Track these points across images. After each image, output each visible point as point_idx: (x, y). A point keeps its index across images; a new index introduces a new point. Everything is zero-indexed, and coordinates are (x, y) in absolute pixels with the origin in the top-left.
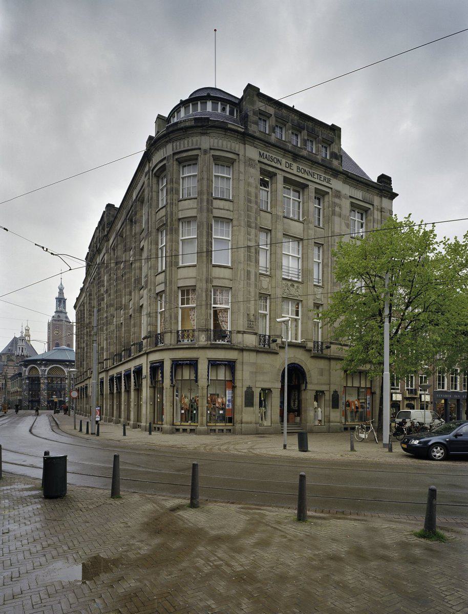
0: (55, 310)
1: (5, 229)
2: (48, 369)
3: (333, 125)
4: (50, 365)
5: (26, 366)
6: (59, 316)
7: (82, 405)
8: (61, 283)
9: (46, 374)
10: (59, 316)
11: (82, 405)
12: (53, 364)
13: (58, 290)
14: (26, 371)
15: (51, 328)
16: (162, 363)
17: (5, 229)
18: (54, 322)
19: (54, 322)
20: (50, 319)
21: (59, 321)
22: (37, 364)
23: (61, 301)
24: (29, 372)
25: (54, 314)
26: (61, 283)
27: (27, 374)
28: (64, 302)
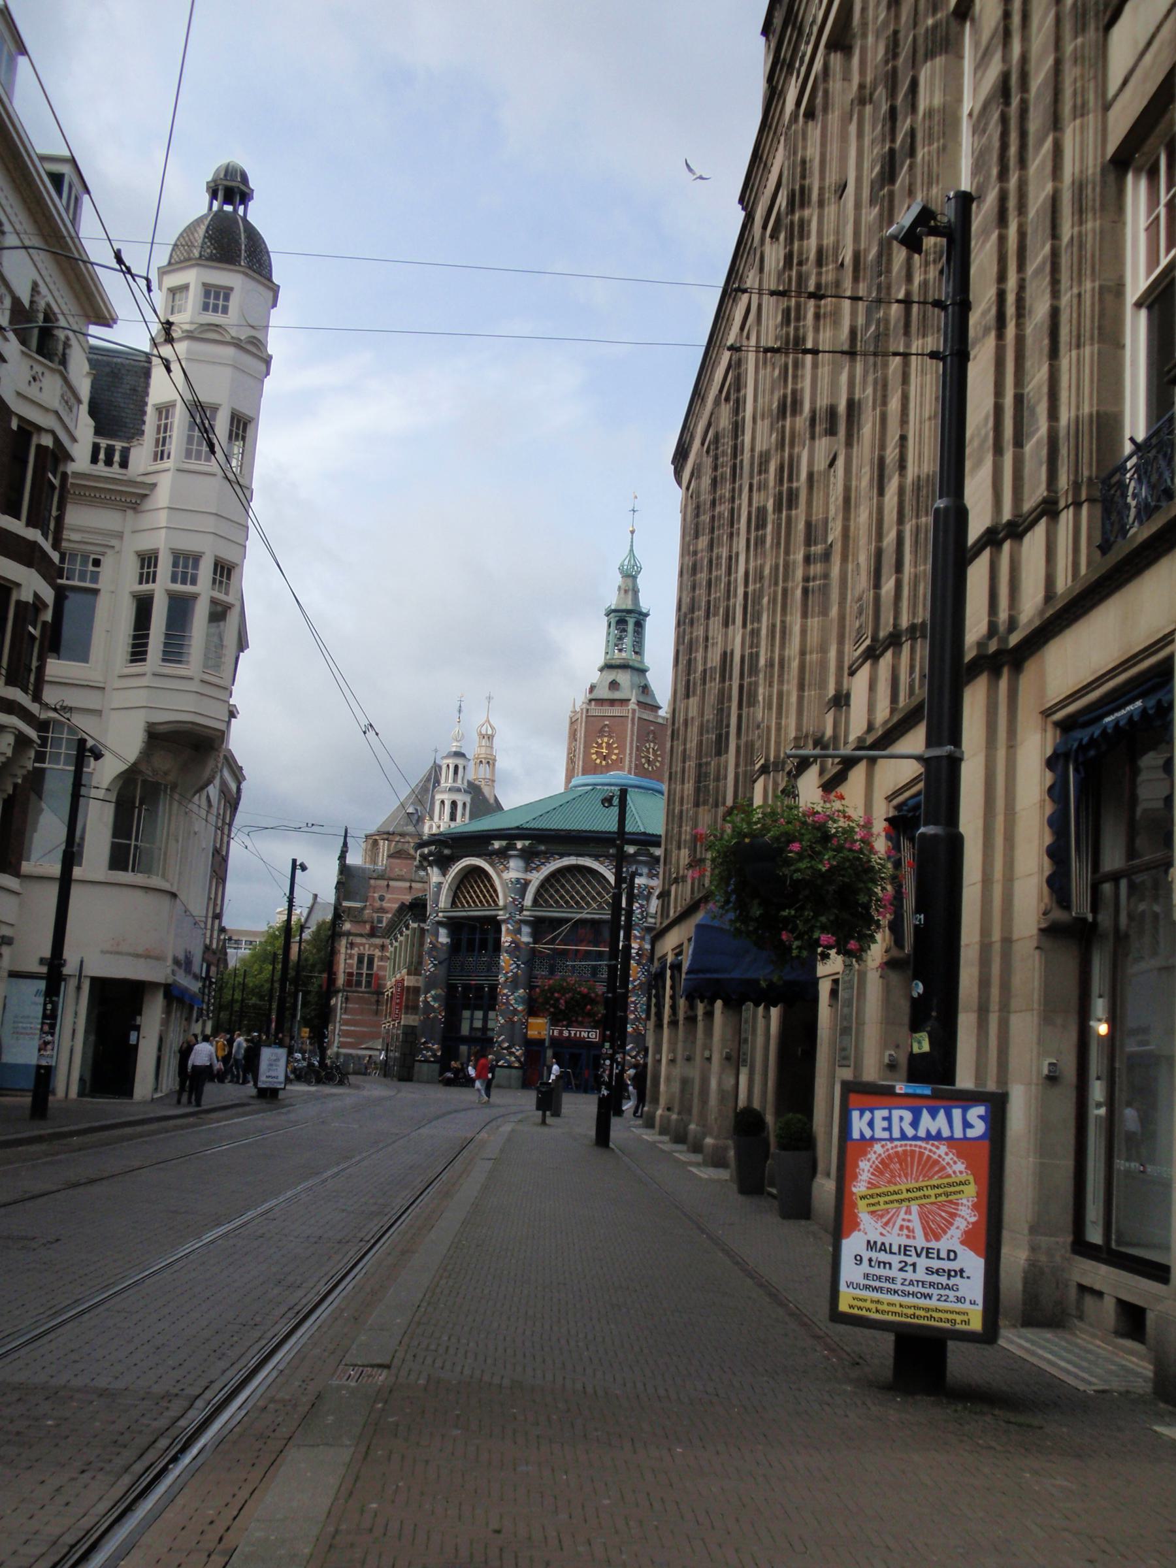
0: (601, 662)
1: (460, 711)
2: (536, 878)
3: (673, 463)
4: (548, 856)
5: (443, 864)
6: (614, 685)
7: (695, 1073)
8: (632, 550)
9: (528, 901)
10: (614, 685)
11: (695, 1073)
12: (562, 856)
13: (618, 579)
14: (439, 884)
15: (581, 734)
16: (185, 288)
17: (460, 711)
18: (596, 711)
19: (596, 711)
20: (580, 698)
21: (612, 702)
22: (489, 855)
23: (628, 621)
24: (455, 896)
25: (595, 677)
26: (632, 550)
27: (444, 901)
28: (639, 625)
